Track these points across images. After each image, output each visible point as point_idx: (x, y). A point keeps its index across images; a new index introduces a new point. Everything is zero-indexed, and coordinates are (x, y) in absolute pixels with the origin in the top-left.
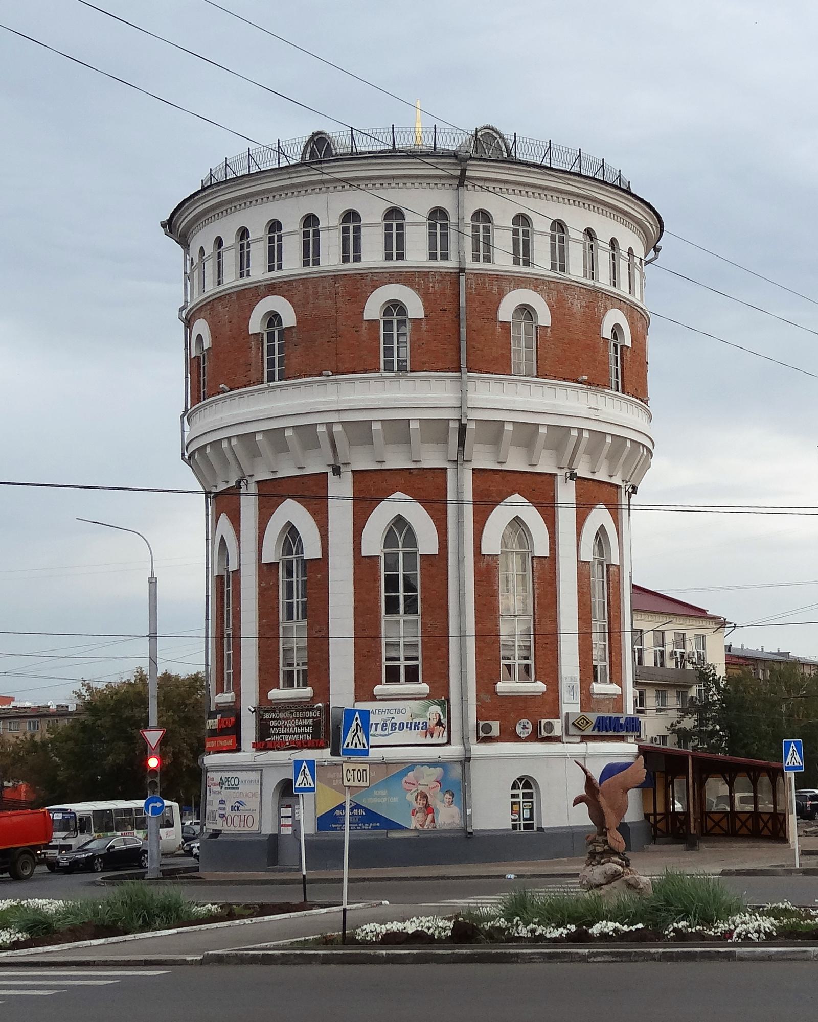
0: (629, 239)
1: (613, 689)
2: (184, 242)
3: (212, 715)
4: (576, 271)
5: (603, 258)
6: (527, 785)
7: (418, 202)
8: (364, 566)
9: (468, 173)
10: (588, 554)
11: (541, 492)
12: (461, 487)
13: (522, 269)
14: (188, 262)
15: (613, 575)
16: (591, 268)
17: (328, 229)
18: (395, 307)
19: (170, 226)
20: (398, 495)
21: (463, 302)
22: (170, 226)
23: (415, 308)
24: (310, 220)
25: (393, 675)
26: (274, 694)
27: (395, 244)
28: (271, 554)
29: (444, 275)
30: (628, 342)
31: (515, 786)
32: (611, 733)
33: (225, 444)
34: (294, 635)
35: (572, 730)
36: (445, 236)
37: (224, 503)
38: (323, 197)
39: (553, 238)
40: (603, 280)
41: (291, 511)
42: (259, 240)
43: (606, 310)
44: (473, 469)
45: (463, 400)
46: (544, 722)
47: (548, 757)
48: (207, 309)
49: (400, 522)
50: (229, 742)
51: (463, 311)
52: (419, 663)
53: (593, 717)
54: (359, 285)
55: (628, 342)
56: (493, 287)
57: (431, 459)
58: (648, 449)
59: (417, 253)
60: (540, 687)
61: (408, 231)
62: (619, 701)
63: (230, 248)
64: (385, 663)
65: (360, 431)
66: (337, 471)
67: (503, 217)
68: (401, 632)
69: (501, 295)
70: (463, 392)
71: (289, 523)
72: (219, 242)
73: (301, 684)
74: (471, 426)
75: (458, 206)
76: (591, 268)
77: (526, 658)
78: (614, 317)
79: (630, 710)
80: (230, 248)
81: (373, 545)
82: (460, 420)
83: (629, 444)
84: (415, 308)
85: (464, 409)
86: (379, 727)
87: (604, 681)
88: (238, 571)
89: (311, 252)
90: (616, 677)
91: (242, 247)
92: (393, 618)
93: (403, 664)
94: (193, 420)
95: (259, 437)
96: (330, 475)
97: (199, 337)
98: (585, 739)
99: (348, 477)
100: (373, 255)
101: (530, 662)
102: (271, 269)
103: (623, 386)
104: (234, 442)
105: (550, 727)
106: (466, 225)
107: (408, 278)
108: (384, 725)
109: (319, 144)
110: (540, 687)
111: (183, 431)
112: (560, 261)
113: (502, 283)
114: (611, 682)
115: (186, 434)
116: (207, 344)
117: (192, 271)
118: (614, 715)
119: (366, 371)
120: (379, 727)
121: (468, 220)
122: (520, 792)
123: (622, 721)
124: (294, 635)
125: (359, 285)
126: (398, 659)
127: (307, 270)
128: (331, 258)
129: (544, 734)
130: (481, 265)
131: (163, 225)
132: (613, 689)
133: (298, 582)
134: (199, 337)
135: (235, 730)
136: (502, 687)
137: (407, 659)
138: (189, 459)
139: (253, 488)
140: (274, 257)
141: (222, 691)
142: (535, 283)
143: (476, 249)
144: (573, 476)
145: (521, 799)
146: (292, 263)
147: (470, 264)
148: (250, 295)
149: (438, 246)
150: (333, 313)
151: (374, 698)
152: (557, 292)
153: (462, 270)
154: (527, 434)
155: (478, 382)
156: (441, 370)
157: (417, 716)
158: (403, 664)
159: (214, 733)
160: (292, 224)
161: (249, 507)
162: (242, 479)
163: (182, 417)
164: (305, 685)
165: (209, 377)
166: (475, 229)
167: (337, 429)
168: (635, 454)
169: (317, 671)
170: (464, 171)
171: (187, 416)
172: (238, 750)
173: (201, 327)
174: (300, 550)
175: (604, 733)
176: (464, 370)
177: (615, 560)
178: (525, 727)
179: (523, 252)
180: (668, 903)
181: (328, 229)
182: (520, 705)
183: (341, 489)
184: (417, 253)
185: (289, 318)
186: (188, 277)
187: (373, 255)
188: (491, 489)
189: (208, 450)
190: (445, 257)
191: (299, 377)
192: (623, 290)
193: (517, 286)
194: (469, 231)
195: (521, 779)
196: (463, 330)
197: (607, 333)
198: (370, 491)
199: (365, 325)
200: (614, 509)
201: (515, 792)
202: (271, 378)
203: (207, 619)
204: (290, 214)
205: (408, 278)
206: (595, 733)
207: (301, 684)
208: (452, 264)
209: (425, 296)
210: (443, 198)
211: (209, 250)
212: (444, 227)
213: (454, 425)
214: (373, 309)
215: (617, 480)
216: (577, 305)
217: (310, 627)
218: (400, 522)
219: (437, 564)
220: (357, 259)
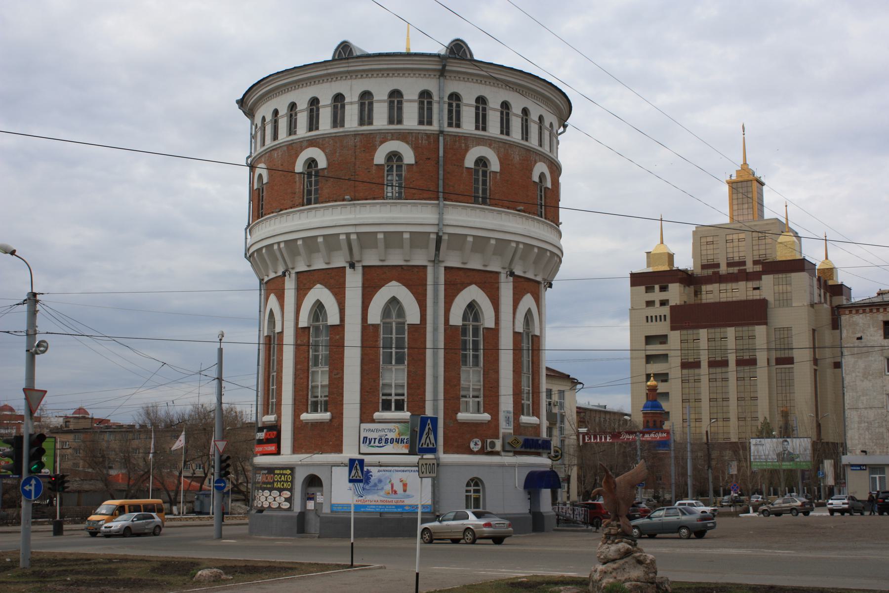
0: (550, 118)
1: (533, 420)
2: (250, 113)
3: (260, 430)
4: (516, 135)
5: (534, 129)
6: (476, 484)
7: (411, 88)
8: (368, 332)
9: (447, 68)
10: (520, 328)
11: (489, 282)
12: (435, 280)
13: (504, 137)
14: (254, 127)
15: (536, 343)
16: (525, 134)
17: (351, 103)
18: (395, 157)
19: (241, 103)
20: (394, 283)
21: (441, 153)
22: (241, 103)
23: (409, 157)
24: (339, 98)
25: (387, 406)
26: (305, 416)
27: (395, 116)
28: (456, 319)
29: (428, 136)
30: (549, 185)
31: (468, 485)
32: (533, 450)
33: (276, 247)
34: (321, 378)
35: (508, 448)
36: (430, 110)
37: (272, 287)
38: (349, 82)
39: (502, 113)
40: (533, 142)
41: (320, 293)
42: (302, 111)
43: (536, 162)
44: (446, 268)
45: (441, 219)
46: (489, 441)
47: (490, 466)
48: (267, 156)
49: (394, 301)
50: (272, 448)
51: (441, 159)
52: (405, 398)
53: (521, 439)
54: (370, 142)
55: (549, 185)
56: (463, 143)
57: (419, 259)
58: (558, 256)
59: (410, 120)
60: (486, 417)
61: (405, 106)
62: (537, 427)
63: (282, 116)
64: (382, 398)
65: (366, 239)
66: (352, 266)
67: (469, 98)
68: (394, 378)
69: (467, 150)
70: (441, 214)
71: (318, 301)
72: (276, 112)
73: (482, 409)
74: (445, 237)
75: (441, 89)
76: (525, 134)
77: (477, 397)
78: (541, 168)
79: (544, 435)
80: (282, 116)
81: (375, 317)
82: (437, 234)
83: (548, 254)
84: (409, 157)
85: (441, 226)
86: (377, 441)
87: (528, 415)
88: (282, 332)
89: (338, 119)
90: (536, 413)
91: (291, 115)
92: (401, 367)
93: (393, 398)
94: (254, 231)
95: (300, 242)
96: (348, 269)
97: (260, 176)
98: (516, 453)
99: (359, 270)
100: (380, 120)
101: (481, 399)
102: (311, 130)
103: (545, 215)
104: (282, 245)
105: (493, 445)
106: (444, 102)
107: (403, 136)
108: (380, 440)
109: (344, 51)
110: (486, 417)
111: (246, 238)
112: (505, 128)
113: (467, 141)
114: (533, 415)
115: (248, 241)
116: (265, 181)
117: (256, 132)
118: (535, 438)
119: (374, 199)
120: (377, 441)
121: (446, 99)
122: (472, 488)
123: (540, 442)
124: (321, 378)
125: (370, 142)
126: (390, 395)
127: (335, 130)
128: (351, 122)
129: (489, 449)
130: (454, 130)
131: (238, 102)
132: (533, 420)
133: (319, 342)
134: (260, 176)
135: (277, 440)
136: (462, 416)
137: (396, 395)
138: (250, 257)
139: (293, 276)
140: (313, 124)
141: (268, 414)
142: (489, 142)
143: (450, 118)
144: (512, 274)
145: (472, 493)
146: (325, 125)
147: (447, 129)
148: (294, 149)
149: (425, 117)
150: (353, 160)
151: (373, 421)
152: (504, 148)
153: (441, 132)
154: (480, 243)
155: (450, 208)
156: (425, 199)
157: (402, 434)
158: (393, 398)
159: (260, 442)
160: (326, 100)
161: (290, 286)
162: (287, 270)
163: (246, 229)
164: (326, 410)
165: (262, 204)
166: (450, 105)
167: (353, 237)
168: (552, 258)
169: (334, 402)
170: (444, 66)
171: (249, 228)
172: (278, 453)
173: (262, 170)
174: (325, 318)
175: (528, 450)
176: (441, 199)
177: (537, 333)
178: (476, 444)
179: (481, 121)
180: (98, 459)
181: (351, 103)
182: (474, 428)
183: (354, 282)
184: (410, 120)
185: (322, 163)
186: (253, 137)
187: (380, 120)
188: (456, 280)
189: (264, 251)
190: (430, 123)
191: (329, 202)
192: (546, 149)
193: (478, 144)
194: (446, 106)
195: (472, 480)
196: (441, 172)
197: (536, 178)
198: (373, 280)
199: (374, 168)
200: (538, 299)
201: (469, 488)
202: (309, 203)
203: (258, 365)
204: (325, 93)
205: (403, 136)
206: (523, 450)
207: (482, 409)
208: (435, 127)
209: (416, 148)
210: (431, 84)
211: (269, 118)
212: (430, 103)
213: (433, 236)
214: (380, 158)
215: (539, 279)
216: (517, 159)
217: (330, 371)
218: (394, 301)
219: (418, 331)
220: (371, 123)
